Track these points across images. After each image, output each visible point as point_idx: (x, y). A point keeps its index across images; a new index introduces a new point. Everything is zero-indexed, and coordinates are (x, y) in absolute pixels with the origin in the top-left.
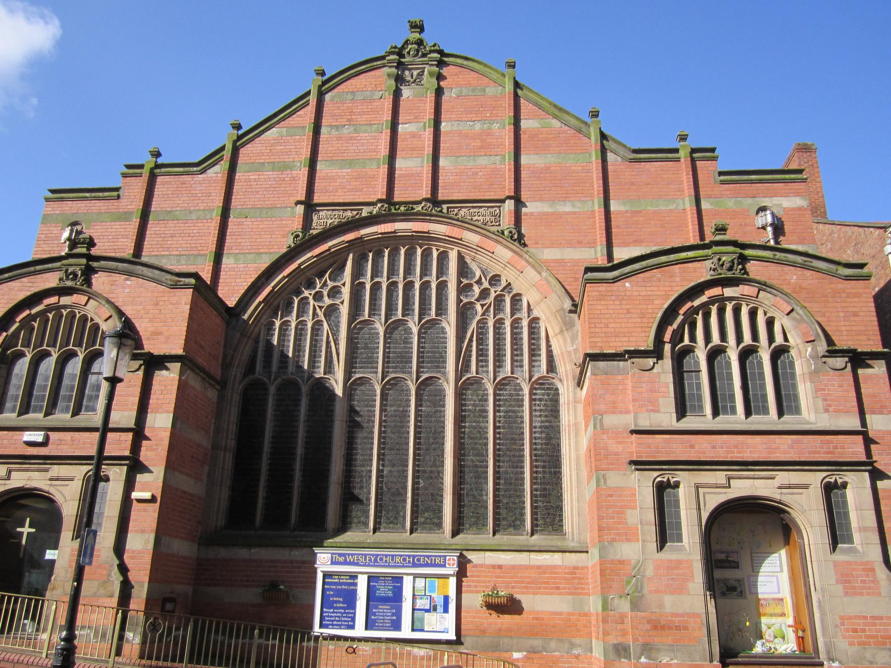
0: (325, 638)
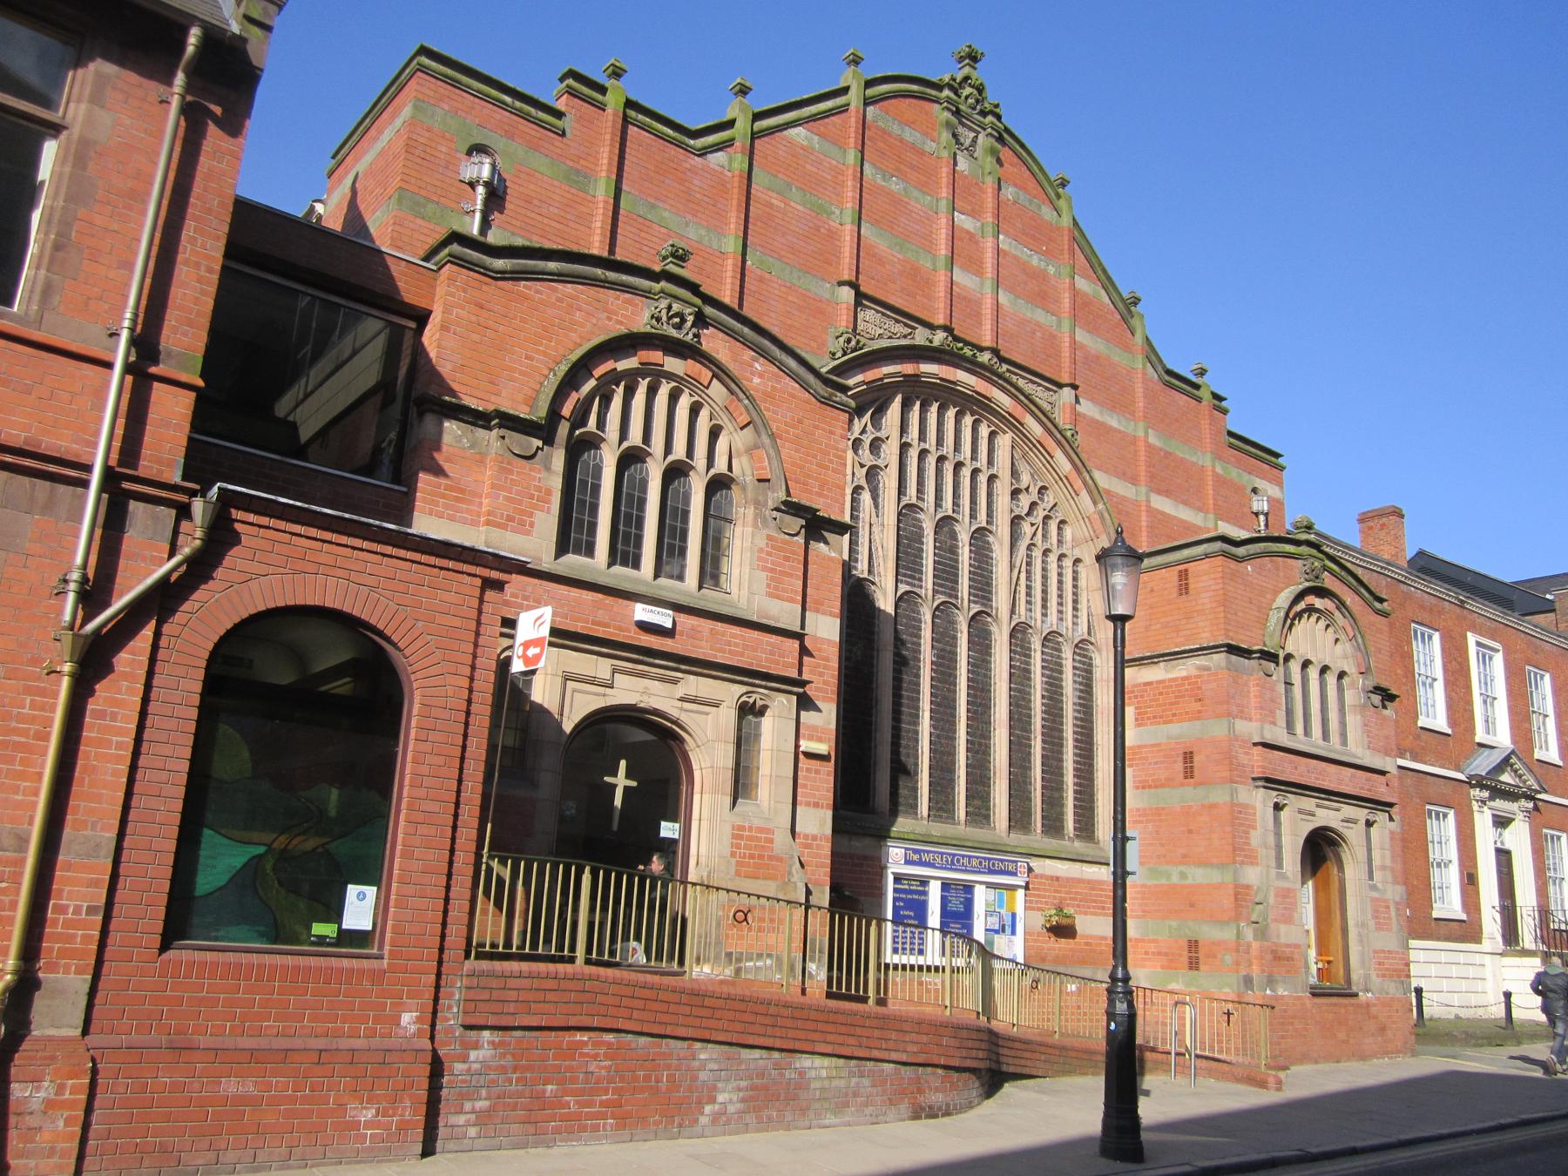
0: (896, 967)
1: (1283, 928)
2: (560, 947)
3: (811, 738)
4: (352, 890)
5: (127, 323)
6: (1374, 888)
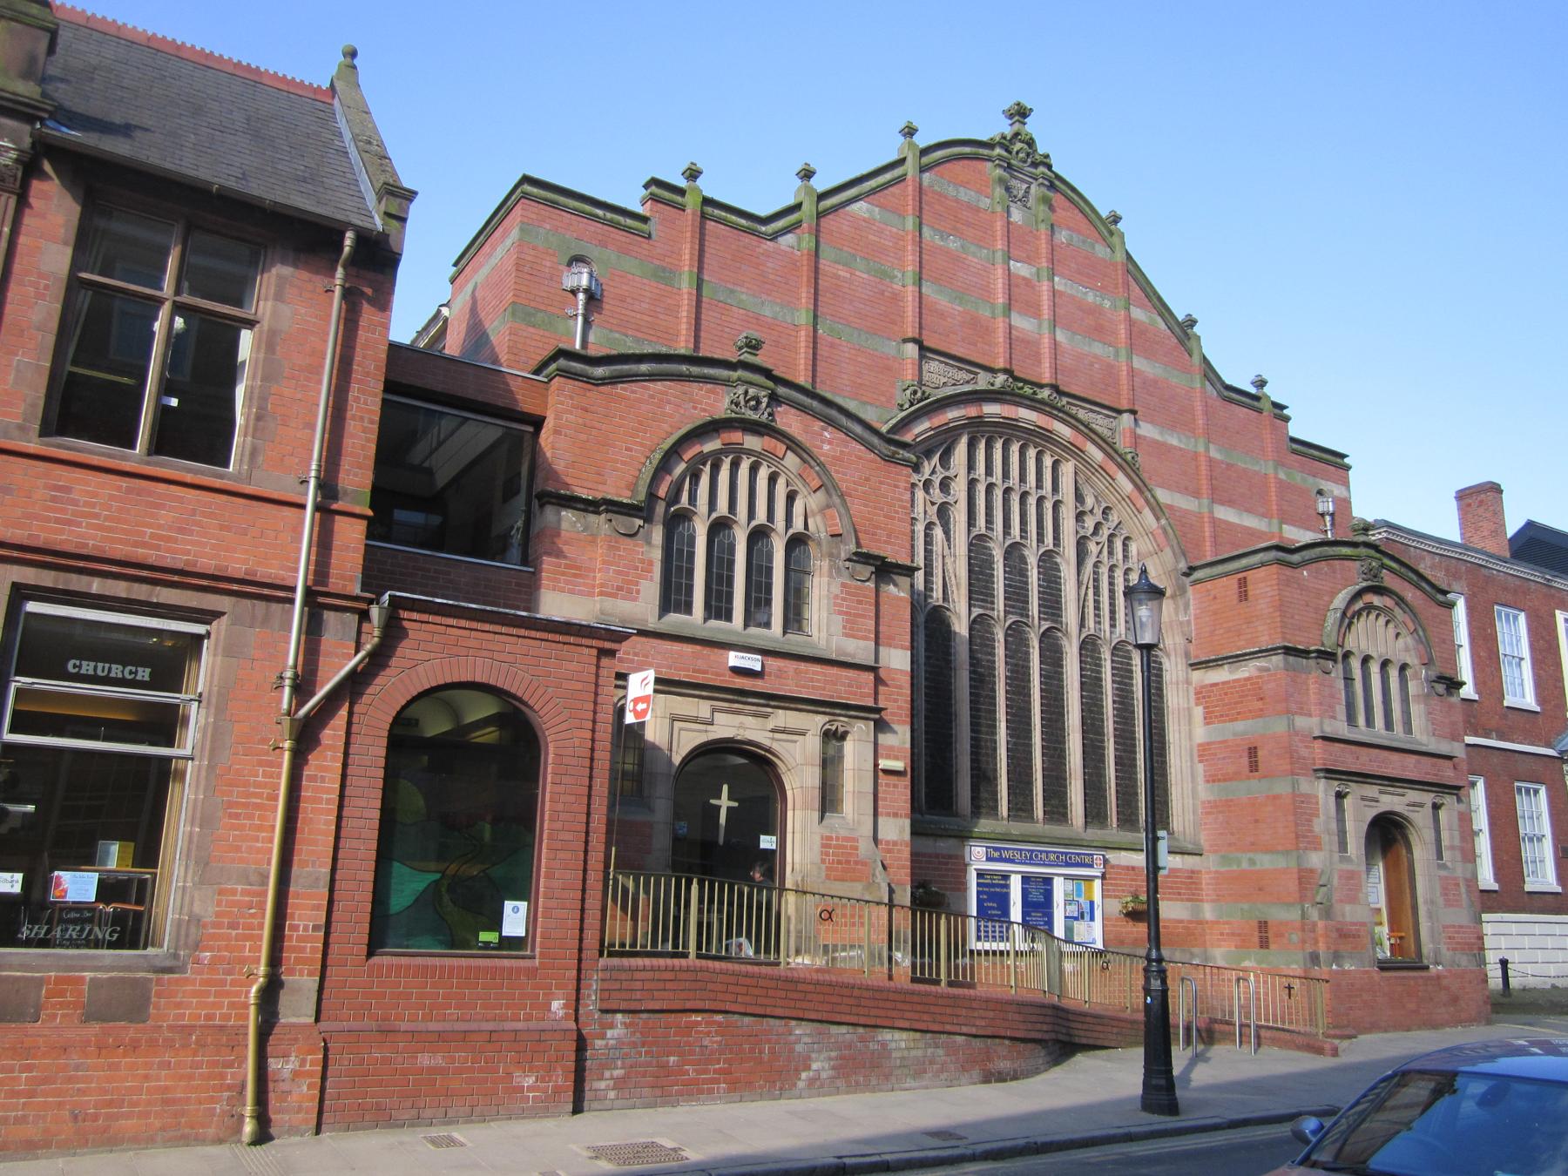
0: (979, 953)
1: (1348, 908)
2: (676, 946)
3: (888, 757)
4: (509, 905)
5: (313, 474)
6: (1444, 867)
